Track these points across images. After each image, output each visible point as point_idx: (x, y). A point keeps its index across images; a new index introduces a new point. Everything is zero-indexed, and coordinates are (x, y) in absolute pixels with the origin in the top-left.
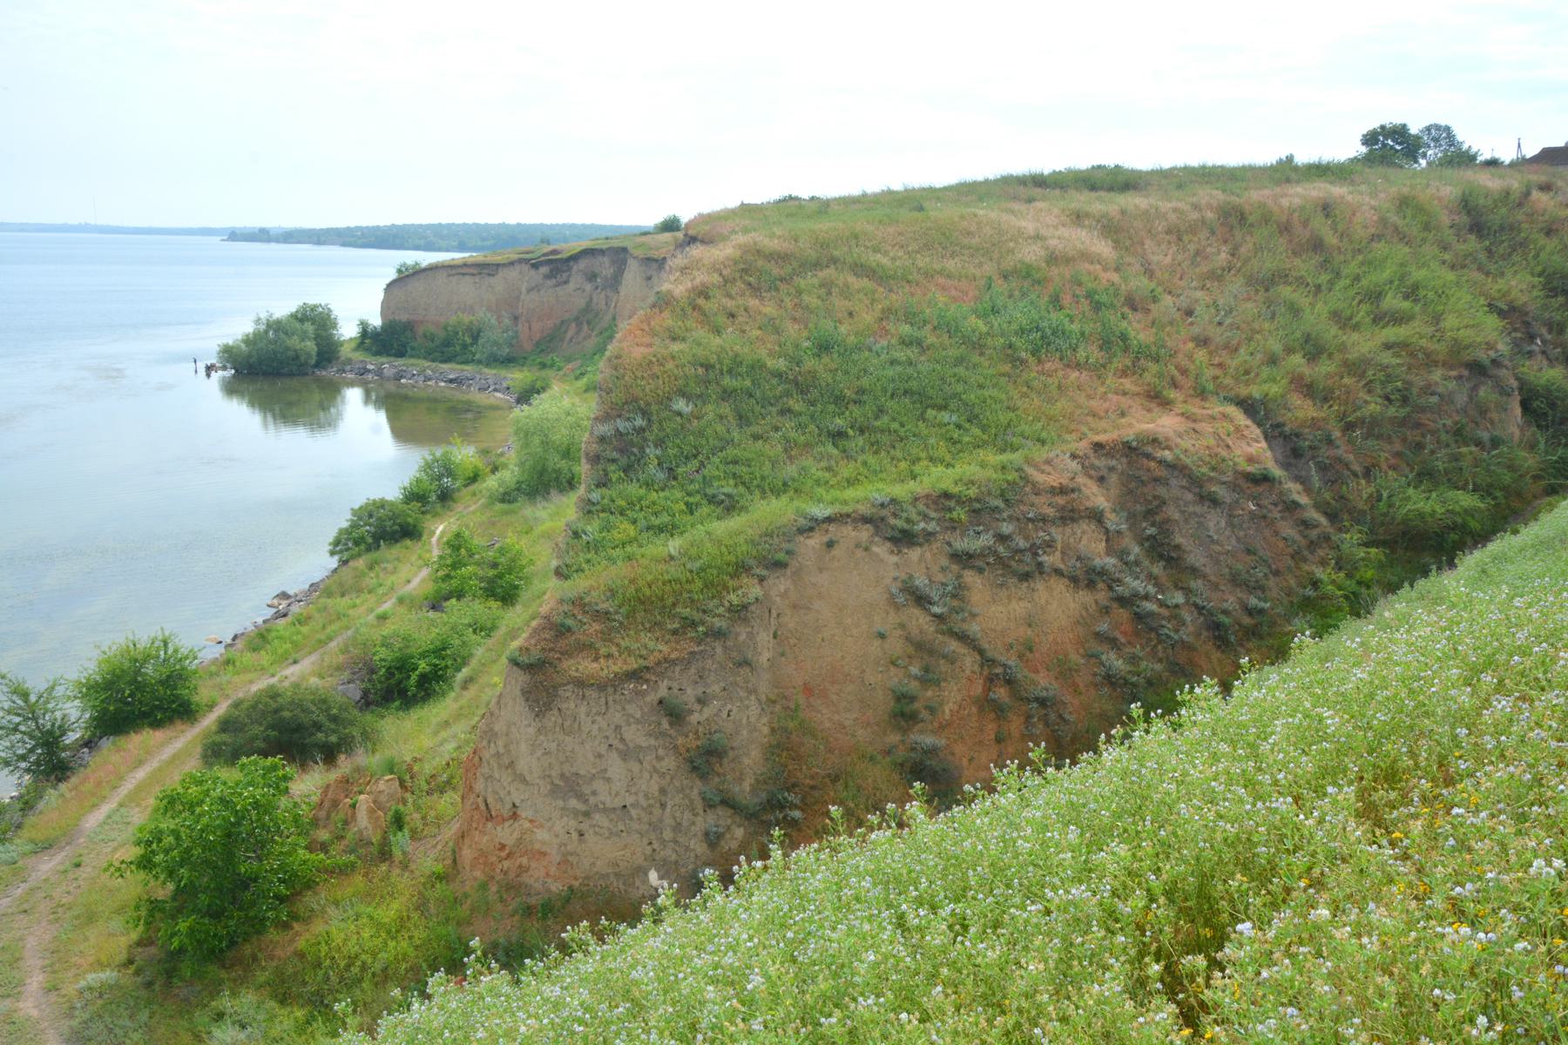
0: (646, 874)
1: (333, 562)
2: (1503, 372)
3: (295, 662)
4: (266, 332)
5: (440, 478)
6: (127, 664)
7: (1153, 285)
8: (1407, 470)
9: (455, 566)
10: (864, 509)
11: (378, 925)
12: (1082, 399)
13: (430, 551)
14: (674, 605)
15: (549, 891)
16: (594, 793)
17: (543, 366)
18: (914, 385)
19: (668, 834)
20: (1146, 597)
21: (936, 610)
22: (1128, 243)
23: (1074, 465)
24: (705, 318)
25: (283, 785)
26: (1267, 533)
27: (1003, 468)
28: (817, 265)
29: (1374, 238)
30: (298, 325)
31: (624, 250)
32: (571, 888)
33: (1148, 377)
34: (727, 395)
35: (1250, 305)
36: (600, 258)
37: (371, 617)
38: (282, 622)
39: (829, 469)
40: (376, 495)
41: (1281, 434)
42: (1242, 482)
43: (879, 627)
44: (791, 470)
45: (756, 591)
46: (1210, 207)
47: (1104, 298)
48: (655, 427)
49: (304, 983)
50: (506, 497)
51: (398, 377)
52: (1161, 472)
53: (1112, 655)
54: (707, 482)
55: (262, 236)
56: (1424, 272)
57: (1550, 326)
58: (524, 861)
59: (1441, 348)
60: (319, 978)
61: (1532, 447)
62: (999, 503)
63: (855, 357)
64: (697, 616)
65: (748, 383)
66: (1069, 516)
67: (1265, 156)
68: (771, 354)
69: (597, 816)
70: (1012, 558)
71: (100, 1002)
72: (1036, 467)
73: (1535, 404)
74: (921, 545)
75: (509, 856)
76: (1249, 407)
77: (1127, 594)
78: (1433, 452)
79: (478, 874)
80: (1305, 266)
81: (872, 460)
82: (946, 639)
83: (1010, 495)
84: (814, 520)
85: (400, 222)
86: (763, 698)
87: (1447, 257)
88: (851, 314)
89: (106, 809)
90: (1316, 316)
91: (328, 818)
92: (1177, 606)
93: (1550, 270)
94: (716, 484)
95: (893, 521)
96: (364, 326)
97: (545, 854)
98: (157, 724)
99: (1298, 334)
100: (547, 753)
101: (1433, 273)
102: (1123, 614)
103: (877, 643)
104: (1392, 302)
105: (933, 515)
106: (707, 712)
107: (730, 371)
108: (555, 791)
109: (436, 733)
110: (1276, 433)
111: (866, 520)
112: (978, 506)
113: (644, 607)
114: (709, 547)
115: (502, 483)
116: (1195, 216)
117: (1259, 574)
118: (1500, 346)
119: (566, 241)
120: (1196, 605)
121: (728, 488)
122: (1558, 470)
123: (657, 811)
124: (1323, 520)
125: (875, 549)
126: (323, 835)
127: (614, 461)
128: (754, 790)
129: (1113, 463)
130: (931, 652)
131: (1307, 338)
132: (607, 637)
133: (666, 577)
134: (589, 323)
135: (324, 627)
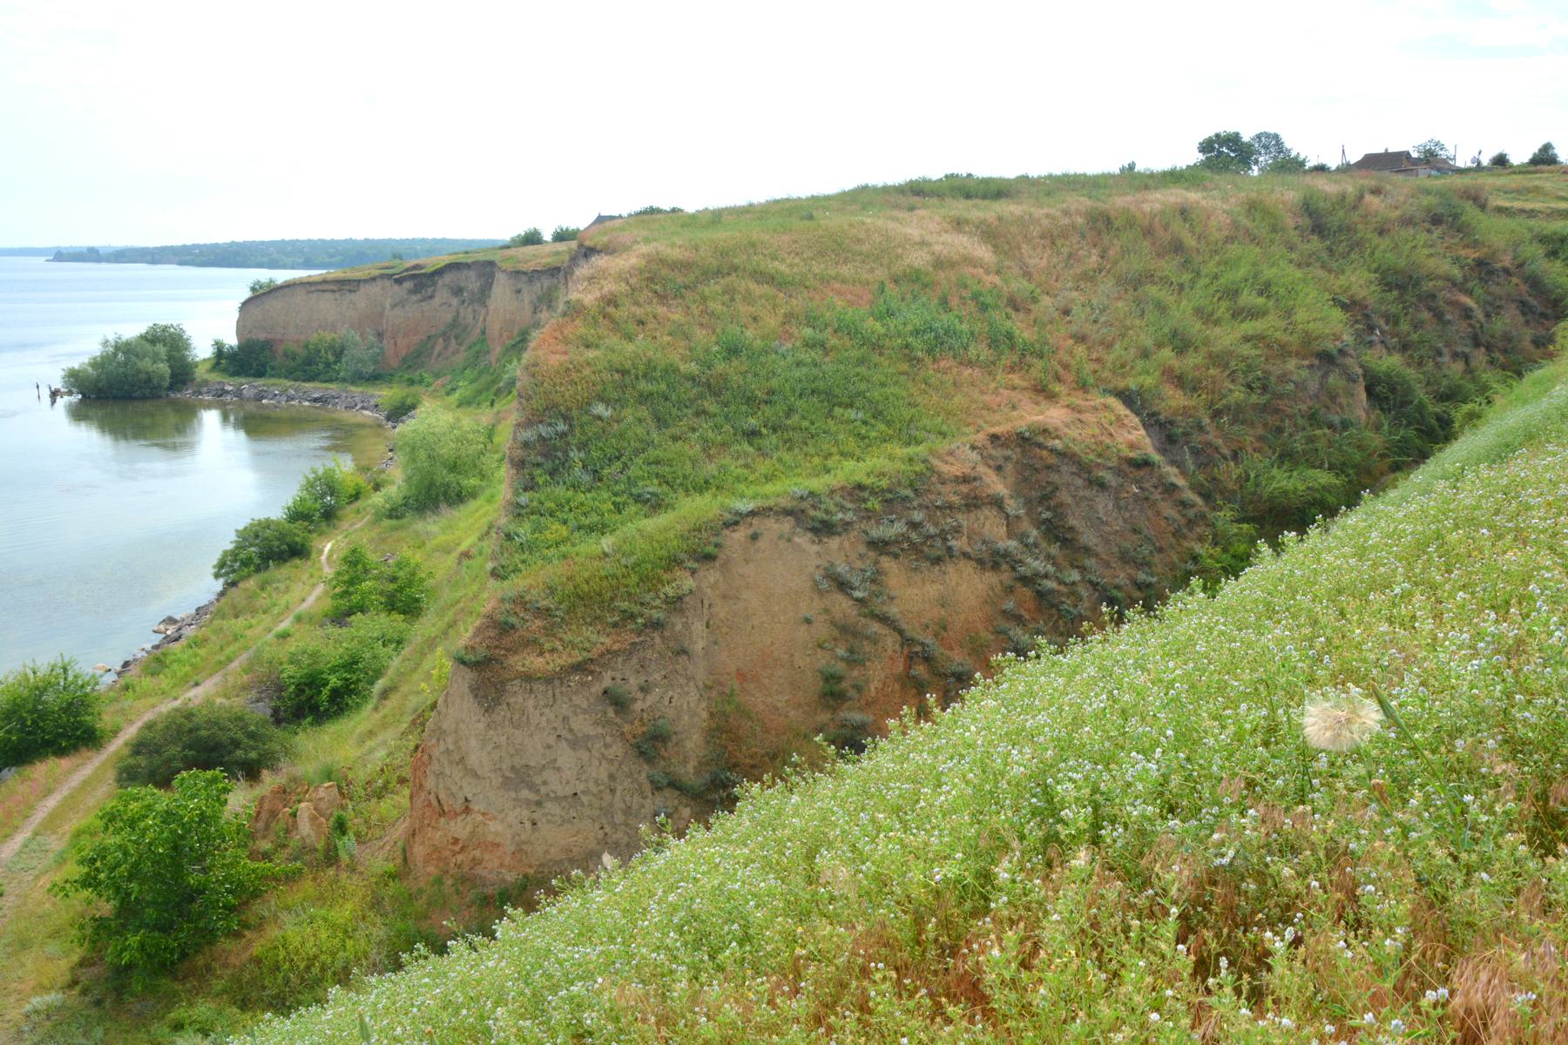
0: (600, 857)
1: (219, 585)
2: (1349, 361)
3: (197, 684)
4: (115, 355)
5: (323, 496)
6: (26, 693)
7: (1032, 287)
8: (1270, 452)
9: (351, 582)
10: (784, 503)
11: (333, 926)
12: (976, 394)
13: (320, 569)
14: (612, 599)
15: (504, 881)
16: (545, 783)
17: (411, 382)
18: (821, 385)
19: (619, 818)
20: (1046, 576)
21: (858, 594)
22: (1006, 247)
23: (974, 456)
24: (615, 325)
25: (223, 797)
26: (1150, 513)
27: (911, 460)
28: (718, 273)
29: (1229, 240)
30: (148, 346)
31: (491, 264)
32: (526, 876)
33: (1034, 372)
34: (644, 398)
35: (1120, 304)
36: (465, 272)
37: (270, 637)
38: (176, 646)
39: (746, 466)
40: (262, 515)
41: (1157, 421)
42: (1125, 467)
43: (805, 613)
44: (711, 469)
45: (689, 583)
46: (1078, 212)
47: (989, 300)
48: (577, 431)
49: (264, 988)
50: (394, 513)
51: (259, 397)
52: (1053, 460)
53: (1019, 631)
54: (631, 482)
55: (92, 255)
56: (1274, 270)
57: (1388, 318)
58: (477, 853)
59: (1293, 340)
60: (279, 981)
61: (1378, 428)
62: (908, 492)
63: (763, 359)
64: (636, 609)
65: (663, 386)
66: (973, 503)
67: (1111, 165)
68: (684, 359)
69: (549, 805)
70: (924, 543)
71: (48, 1023)
72: (939, 457)
73: (1378, 389)
74: (839, 534)
75: (462, 849)
76: (1127, 397)
77: (1029, 573)
78: (1291, 435)
79: (431, 869)
80: (1168, 267)
81: (787, 457)
82: (868, 621)
83: (918, 485)
84: (737, 513)
85: (239, 239)
86: (701, 685)
87: (1293, 256)
88: (755, 319)
89: (19, 839)
90: (1182, 313)
91: (267, 827)
92: (1074, 583)
93: (1384, 267)
94: (640, 484)
95: (812, 513)
96: (219, 346)
97: (498, 845)
98: (61, 752)
99: (1166, 330)
100: (497, 747)
101: (1283, 272)
102: (1026, 593)
103: (804, 628)
104: (1248, 298)
105: (849, 505)
106: (650, 699)
107: (645, 376)
108: (506, 783)
109: (361, 742)
110: (1154, 422)
111: (788, 513)
112: (890, 496)
113: (587, 602)
114: (641, 544)
115: (388, 499)
116: (1066, 221)
117: (1146, 550)
118: (1345, 337)
119: (417, 256)
120: (1091, 582)
121: (653, 487)
122: (1400, 448)
123: (607, 797)
124: (1199, 501)
125: (797, 539)
126: (265, 845)
127: (538, 465)
128: (697, 772)
129: (1009, 452)
130: (855, 634)
131: (1175, 333)
132: (549, 632)
133: (603, 573)
134: (457, 337)
135: (222, 649)
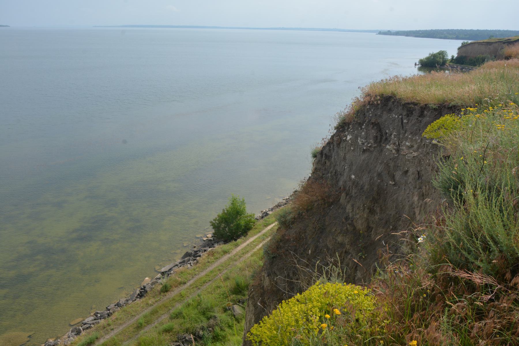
55: (389, 33)
96: (453, 57)
97: (475, 159)
129: (446, 311)
